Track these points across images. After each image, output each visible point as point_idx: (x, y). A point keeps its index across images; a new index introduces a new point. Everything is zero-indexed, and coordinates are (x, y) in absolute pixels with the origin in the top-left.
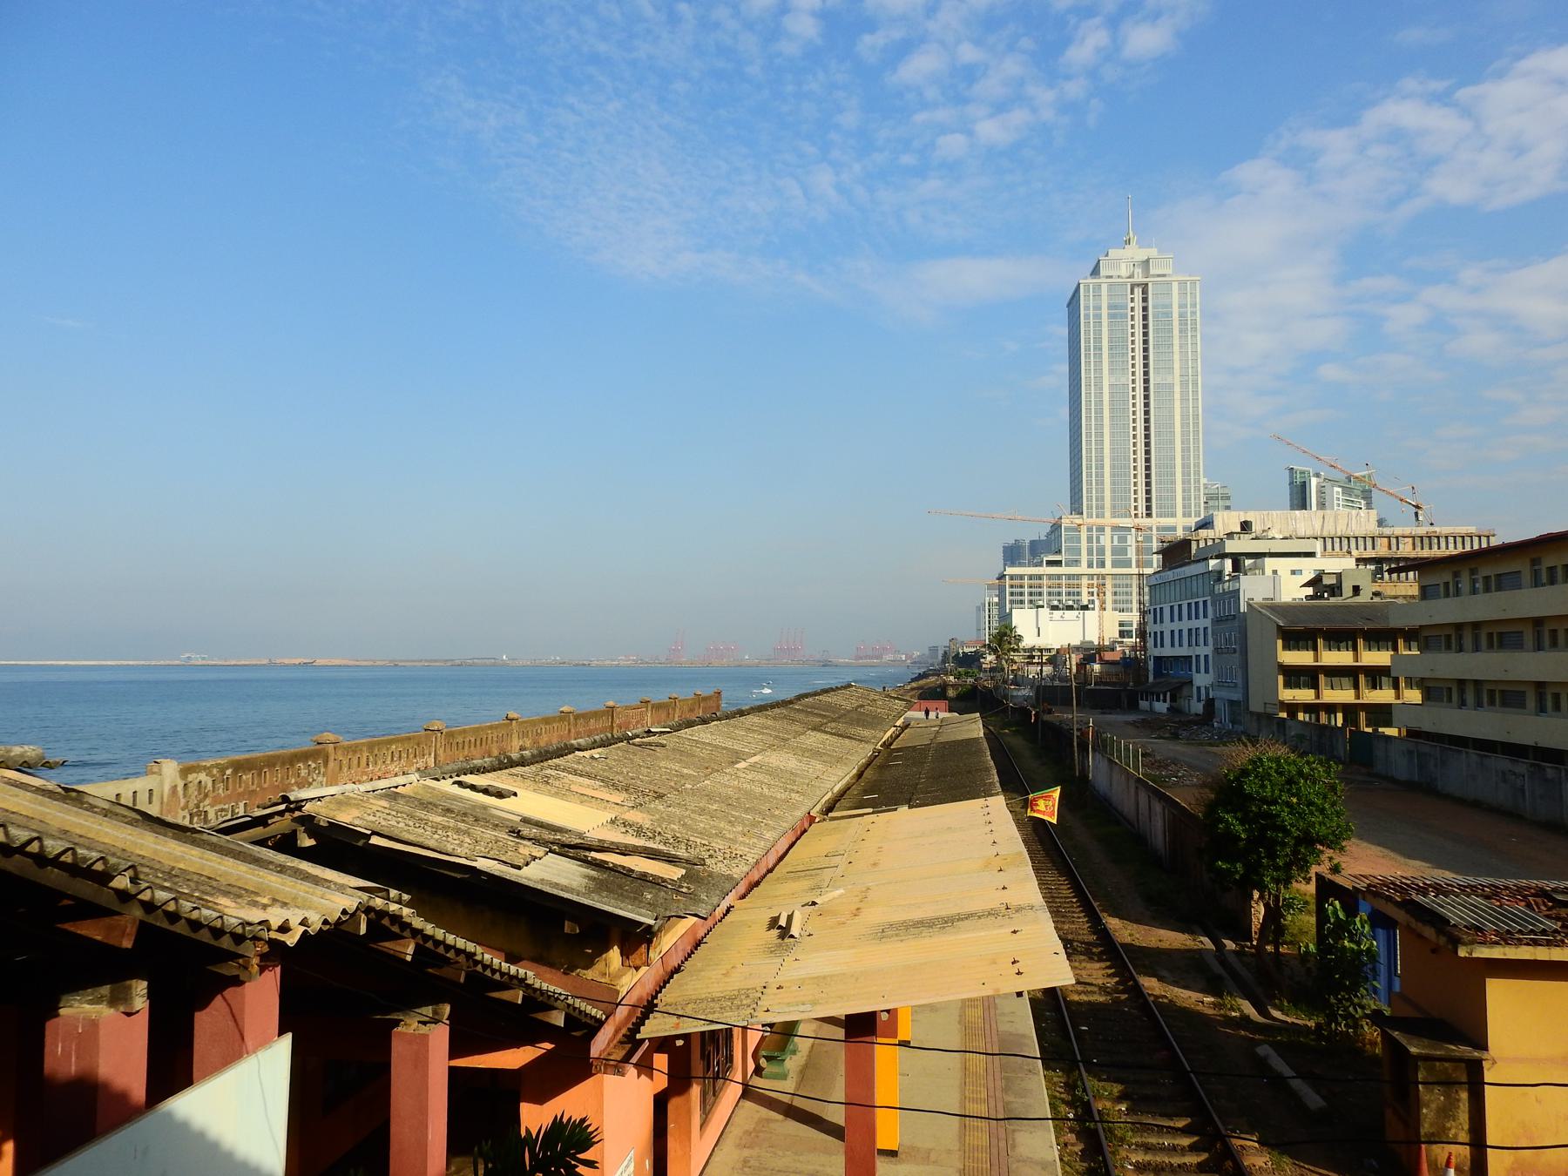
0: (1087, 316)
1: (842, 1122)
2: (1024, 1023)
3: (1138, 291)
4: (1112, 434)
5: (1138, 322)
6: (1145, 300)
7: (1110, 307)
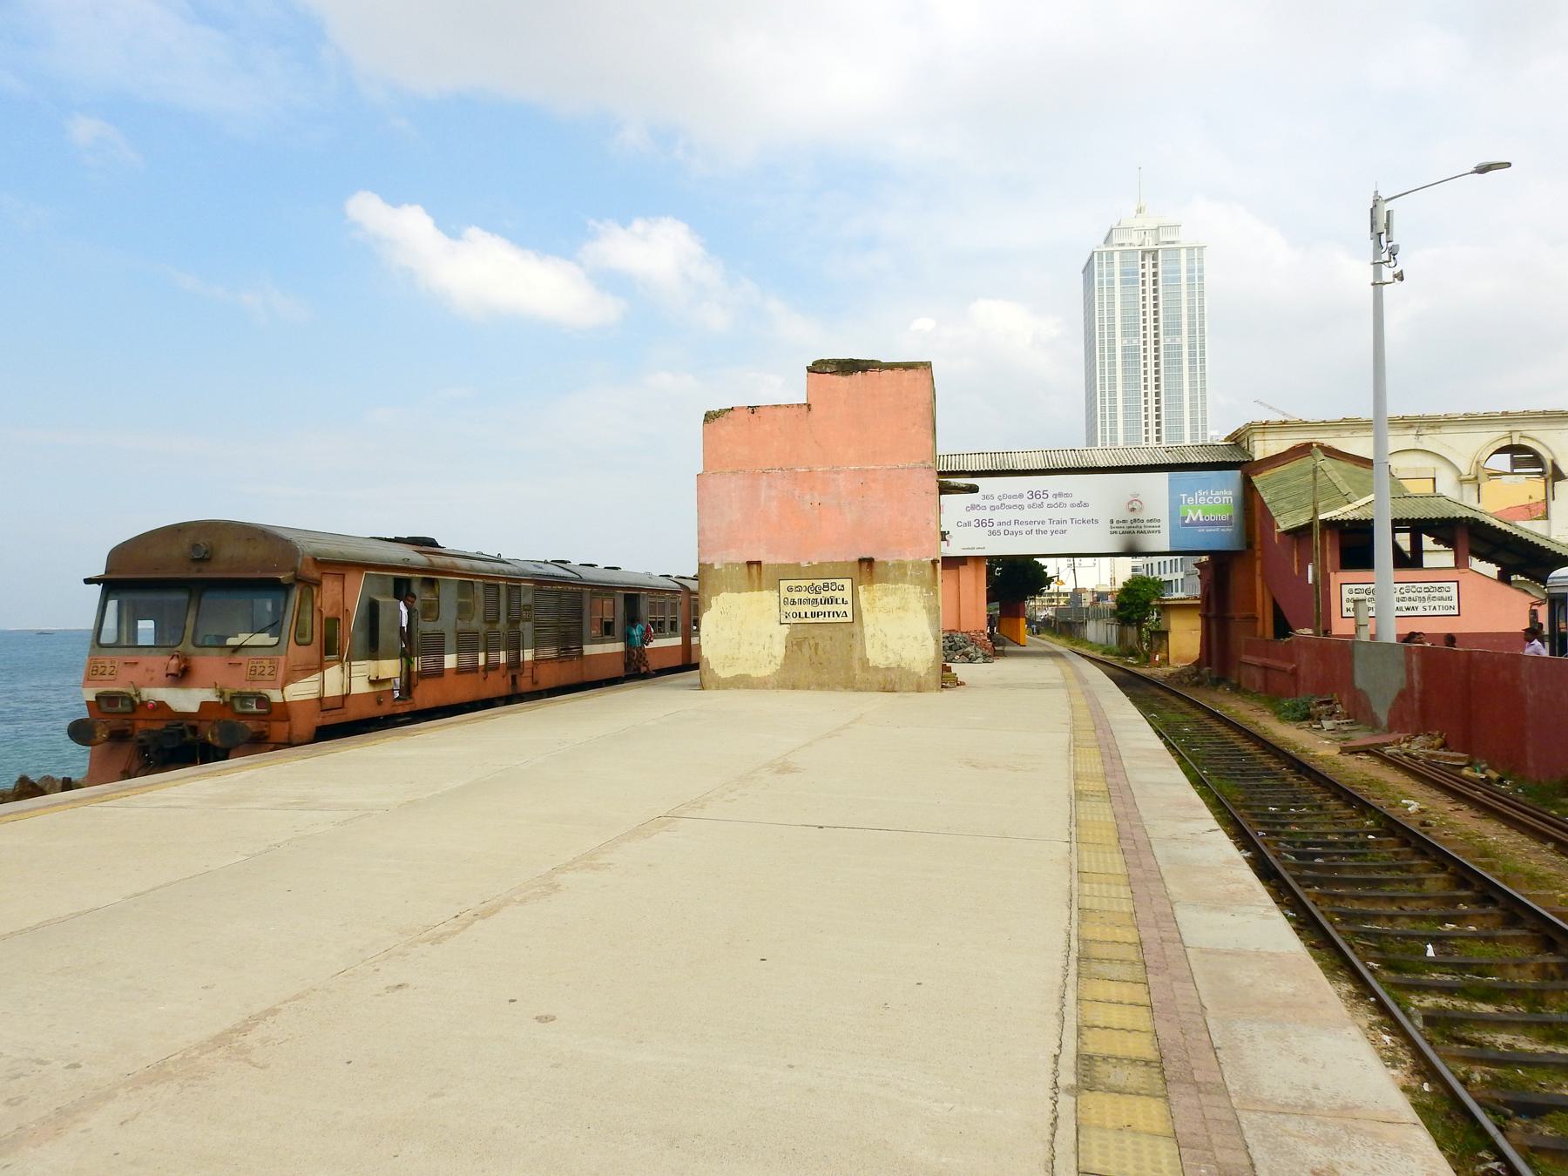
0: (1101, 283)
1: (1371, 457)
2: (1163, 628)
3: (1149, 262)
4: (1125, 393)
5: (1149, 287)
6: (1155, 266)
7: (1123, 273)
